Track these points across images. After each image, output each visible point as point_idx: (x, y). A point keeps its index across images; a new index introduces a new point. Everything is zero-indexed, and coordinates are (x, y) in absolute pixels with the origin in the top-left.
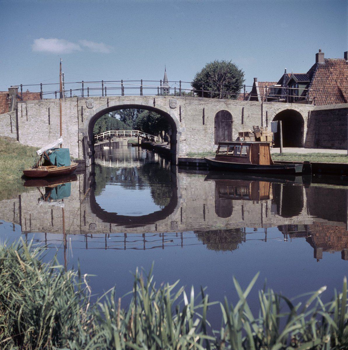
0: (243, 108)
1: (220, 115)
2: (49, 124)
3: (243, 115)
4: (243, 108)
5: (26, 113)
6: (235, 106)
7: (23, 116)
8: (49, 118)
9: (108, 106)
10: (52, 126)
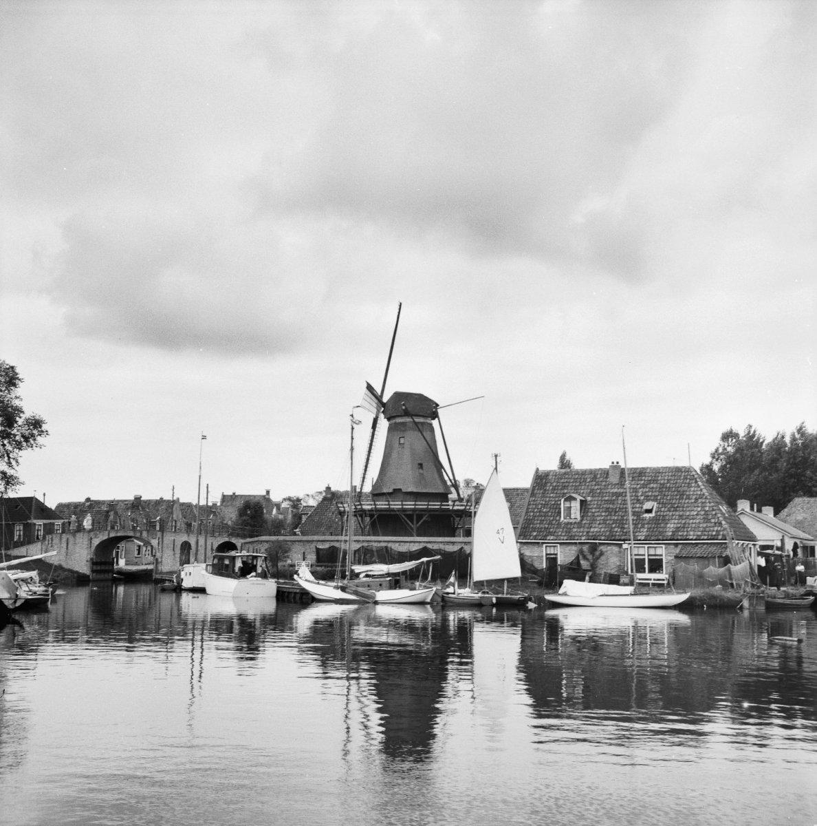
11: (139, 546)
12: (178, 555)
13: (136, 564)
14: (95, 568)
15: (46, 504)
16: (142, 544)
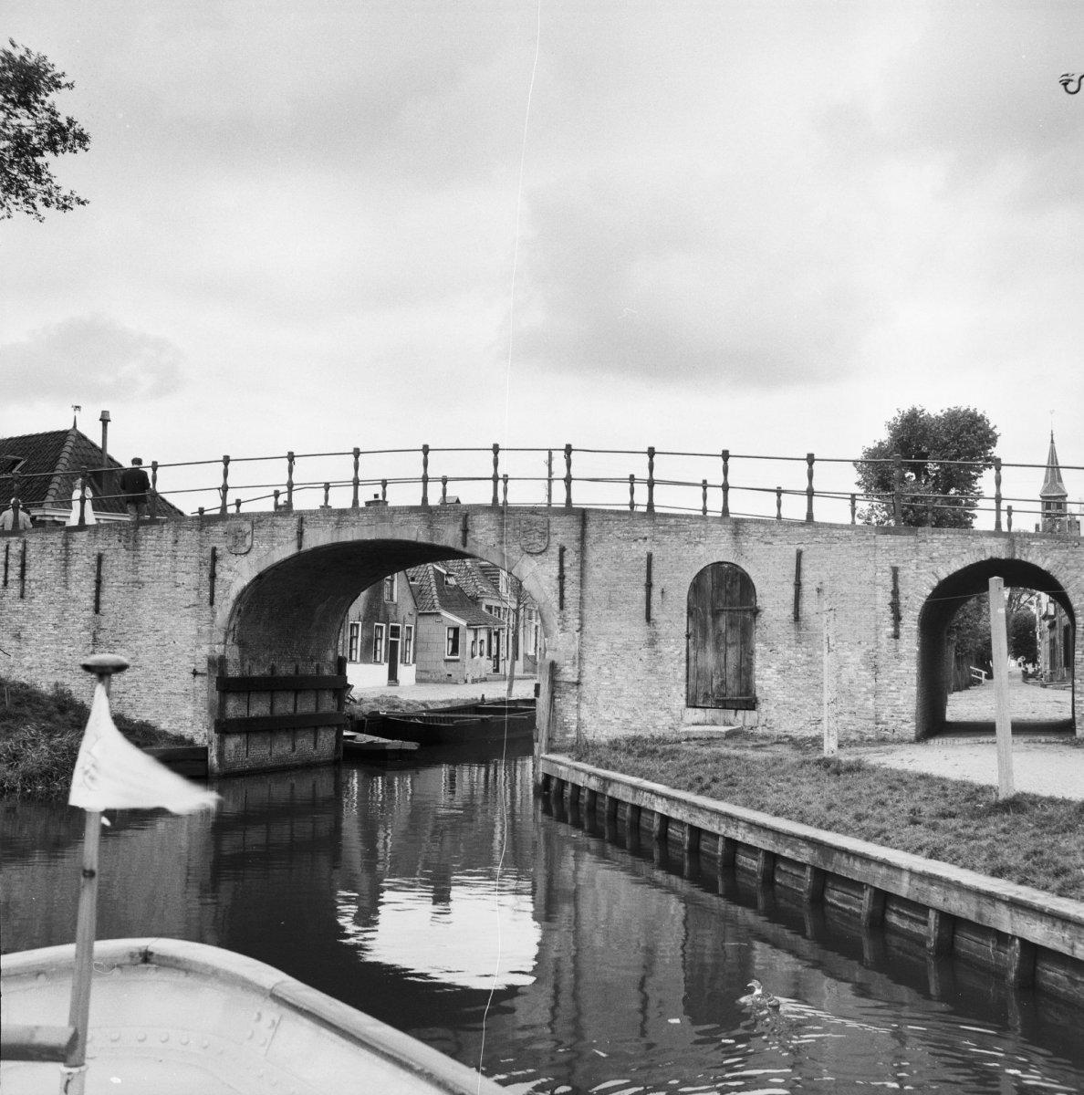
0: (799, 554)
1: (708, 582)
2: (97, 610)
3: (798, 585)
4: (799, 554)
5: (101, 595)
6: (768, 546)
7: (9, 584)
8: (98, 591)
9: (300, 546)
10: (103, 619)
11: (456, 630)
12: (674, 646)
13: (449, 680)
14: (234, 708)
15: (110, 451)
16: (462, 623)
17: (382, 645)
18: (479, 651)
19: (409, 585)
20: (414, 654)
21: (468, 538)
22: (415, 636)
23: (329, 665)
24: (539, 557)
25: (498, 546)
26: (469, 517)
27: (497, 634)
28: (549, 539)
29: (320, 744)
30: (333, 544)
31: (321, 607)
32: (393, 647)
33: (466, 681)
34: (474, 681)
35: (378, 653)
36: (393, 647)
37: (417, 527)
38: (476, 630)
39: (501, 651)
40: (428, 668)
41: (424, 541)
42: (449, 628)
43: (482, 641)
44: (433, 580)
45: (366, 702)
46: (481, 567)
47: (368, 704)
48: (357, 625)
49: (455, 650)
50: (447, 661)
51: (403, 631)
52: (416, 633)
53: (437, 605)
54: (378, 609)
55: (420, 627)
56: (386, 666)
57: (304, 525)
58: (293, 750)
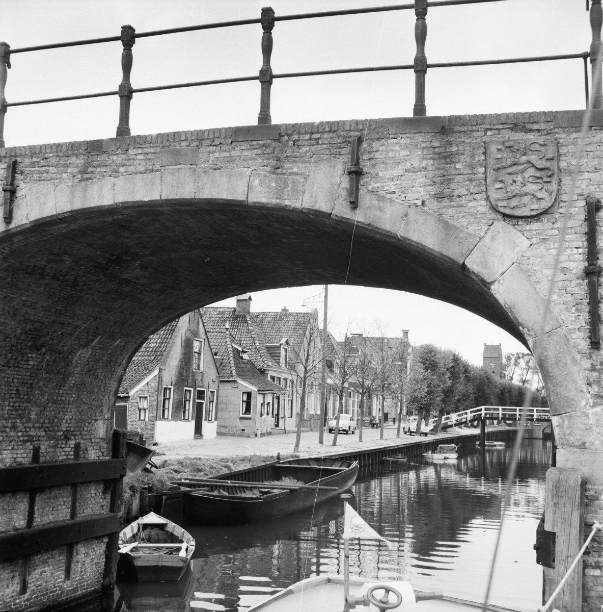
17: (190, 406)
18: (266, 412)
19: (214, 358)
20: (216, 413)
21: (362, 190)
22: (217, 399)
23: (97, 443)
24: (535, 226)
25: (433, 205)
26: (364, 145)
27: (278, 398)
28: (560, 182)
29: (76, 568)
30: (83, 209)
31: (82, 355)
32: (199, 408)
33: (256, 435)
34: (263, 435)
35: (187, 412)
36: (199, 408)
37: (247, 171)
38: (264, 395)
39: (280, 412)
40: (227, 424)
41: (264, 200)
42: (243, 393)
43: (268, 404)
44: (231, 355)
45: (170, 465)
46: (267, 348)
47: (172, 467)
48: (170, 389)
49: (248, 410)
50: (241, 418)
51: (207, 395)
52: (217, 396)
53: (234, 374)
54: (187, 376)
55: (220, 392)
56: (193, 422)
57: (18, 176)
58: (24, 590)
